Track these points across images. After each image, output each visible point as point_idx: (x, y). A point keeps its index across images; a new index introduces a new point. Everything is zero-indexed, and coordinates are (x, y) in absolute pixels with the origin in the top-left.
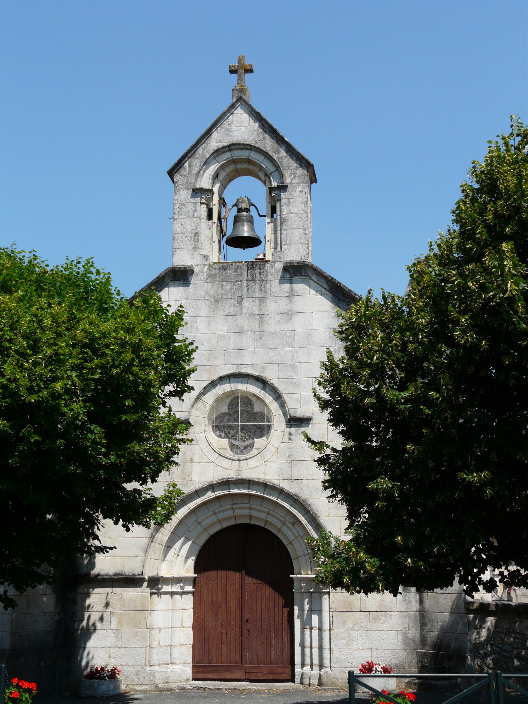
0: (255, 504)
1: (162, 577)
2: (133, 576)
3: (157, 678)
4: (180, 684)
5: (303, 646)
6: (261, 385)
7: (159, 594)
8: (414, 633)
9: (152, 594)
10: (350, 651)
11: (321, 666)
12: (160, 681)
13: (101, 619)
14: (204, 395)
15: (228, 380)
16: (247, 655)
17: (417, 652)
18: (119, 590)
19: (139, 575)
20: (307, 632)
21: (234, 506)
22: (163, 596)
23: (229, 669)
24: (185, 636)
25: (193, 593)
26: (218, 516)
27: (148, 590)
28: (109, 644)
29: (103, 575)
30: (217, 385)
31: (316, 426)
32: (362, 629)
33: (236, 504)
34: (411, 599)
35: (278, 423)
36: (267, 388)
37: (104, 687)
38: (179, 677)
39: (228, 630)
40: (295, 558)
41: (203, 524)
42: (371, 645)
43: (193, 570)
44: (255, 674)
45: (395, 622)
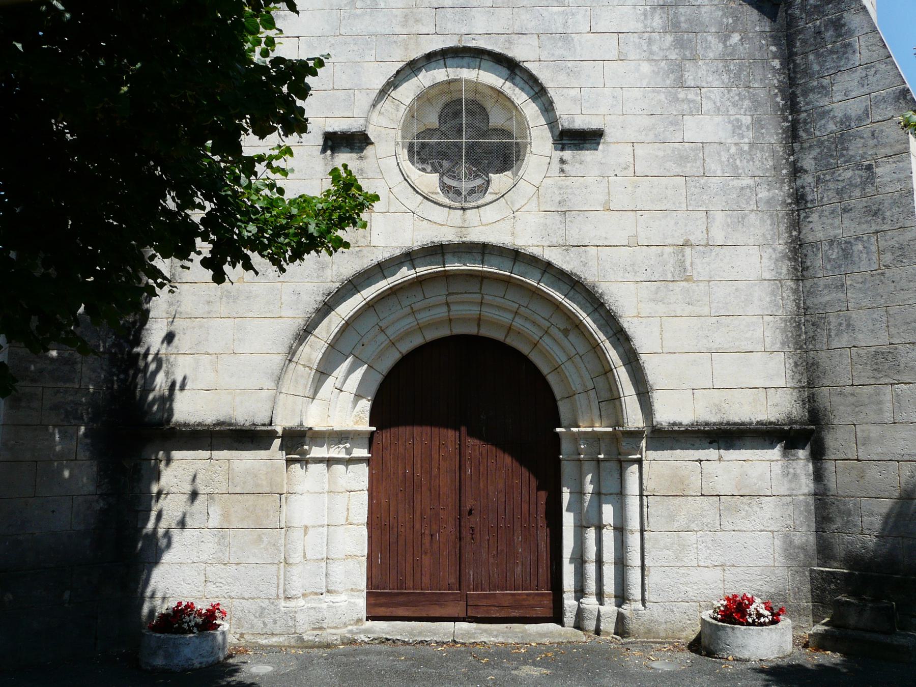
0: (492, 294)
1: (311, 429)
2: (253, 428)
3: (301, 623)
4: (344, 631)
5: (580, 560)
6: (505, 72)
7: (305, 462)
8: (805, 536)
9: (289, 462)
10: (682, 570)
11: (622, 598)
12: (306, 627)
13: (182, 524)
14: (396, 88)
15: (442, 62)
16: (470, 574)
17: (812, 571)
18: (225, 454)
19: (264, 425)
20: (591, 534)
21: (451, 299)
22: (311, 467)
23: (437, 600)
24: (354, 541)
25: (367, 461)
26: (419, 316)
28: (204, 557)
29: (193, 425)
30: (420, 70)
31: (613, 147)
32: (706, 528)
33: (453, 294)
34: (798, 471)
35: (540, 142)
36: (518, 78)
37: (191, 650)
38: (343, 617)
39: (435, 527)
40: (563, 398)
41: (389, 332)
42: (722, 559)
43: (368, 419)
44: (485, 608)
45: (768, 516)
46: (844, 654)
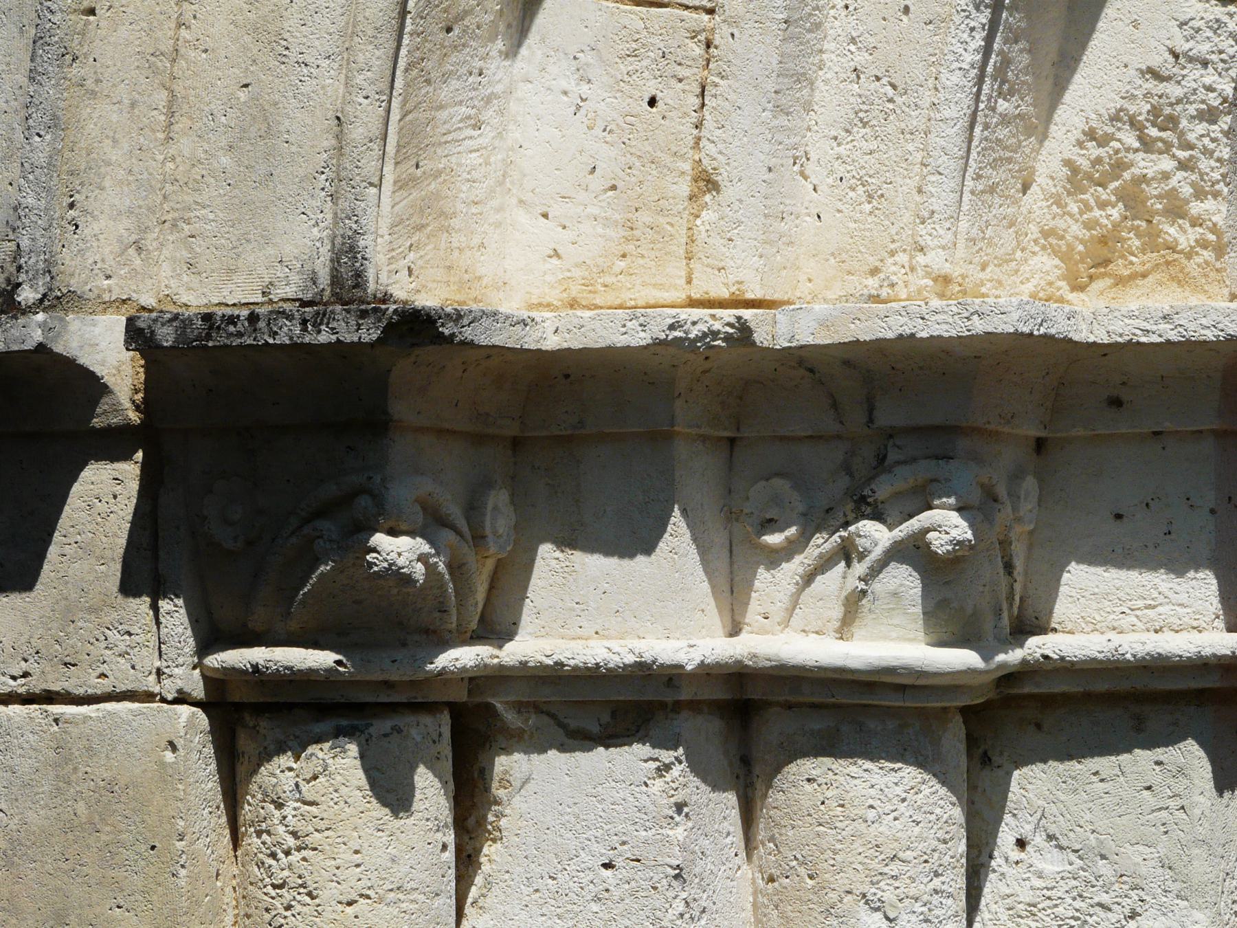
7: (466, 739)
9: (248, 722)
22: (540, 786)
27: (161, 642)
46: (413, 769)
